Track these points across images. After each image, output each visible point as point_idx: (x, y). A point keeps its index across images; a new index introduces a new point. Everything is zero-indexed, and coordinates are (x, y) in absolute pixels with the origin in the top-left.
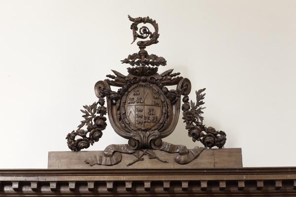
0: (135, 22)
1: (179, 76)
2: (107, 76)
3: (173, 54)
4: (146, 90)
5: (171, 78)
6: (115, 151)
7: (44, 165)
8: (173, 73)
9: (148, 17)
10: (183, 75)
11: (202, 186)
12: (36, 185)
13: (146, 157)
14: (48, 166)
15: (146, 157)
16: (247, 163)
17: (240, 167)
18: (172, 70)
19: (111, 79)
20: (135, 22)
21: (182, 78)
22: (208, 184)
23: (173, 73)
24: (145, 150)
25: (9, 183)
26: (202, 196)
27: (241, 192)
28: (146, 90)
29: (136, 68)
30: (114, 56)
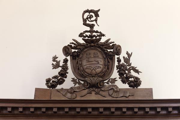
0: (96, 13)
1: (114, 43)
2: (70, 43)
3: (109, 30)
4: (92, 53)
5: (107, 44)
6: (72, 91)
7: (32, 97)
8: (110, 41)
9: (88, 9)
10: (117, 43)
11: (77, 111)
12: (33, 110)
13: (93, 93)
14: (34, 98)
15: (93, 93)
16: (156, 97)
17: (150, 99)
18: (109, 39)
19: (73, 45)
20: (96, 13)
21: (115, 44)
22: (12, 109)
23: (110, 41)
24: (94, 88)
25: (6, 108)
26: (103, 119)
27: (11, 114)
28: (92, 53)
29: (87, 39)
30: (74, 32)
